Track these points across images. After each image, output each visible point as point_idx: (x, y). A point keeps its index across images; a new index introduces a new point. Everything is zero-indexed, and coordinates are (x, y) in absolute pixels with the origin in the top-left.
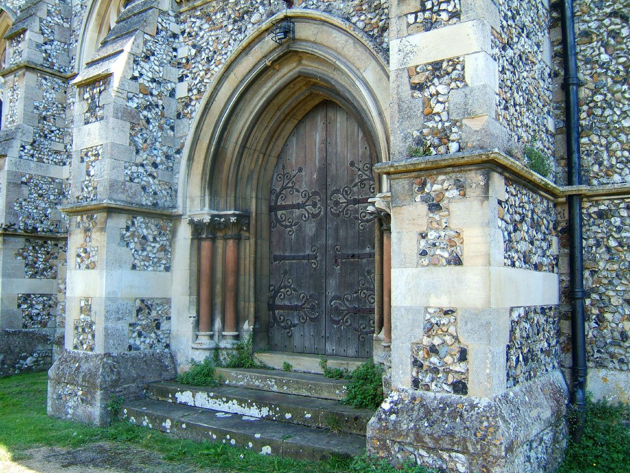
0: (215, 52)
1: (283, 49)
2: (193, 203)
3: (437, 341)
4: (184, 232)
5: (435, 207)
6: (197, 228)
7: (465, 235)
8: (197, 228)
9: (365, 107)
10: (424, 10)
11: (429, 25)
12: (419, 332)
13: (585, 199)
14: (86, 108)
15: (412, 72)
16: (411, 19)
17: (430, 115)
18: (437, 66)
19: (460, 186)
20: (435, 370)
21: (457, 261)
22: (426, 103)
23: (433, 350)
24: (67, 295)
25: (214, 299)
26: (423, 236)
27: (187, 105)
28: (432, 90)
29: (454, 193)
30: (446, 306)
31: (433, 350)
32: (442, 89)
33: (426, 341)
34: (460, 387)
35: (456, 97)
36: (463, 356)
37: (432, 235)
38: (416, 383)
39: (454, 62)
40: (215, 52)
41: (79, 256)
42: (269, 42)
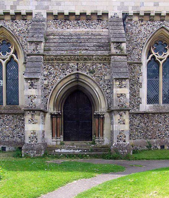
0: (56, 76)
1: (76, 79)
2: (51, 109)
3: (121, 135)
4: (48, 116)
5: (121, 116)
6: (52, 115)
7: (126, 120)
8: (52, 115)
9: (92, 93)
10: (120, 85)
11: (120, 87)
12: (118, 134)
13: (28, 117)
14: (29, 84)
15: (117, 94)
16: (118, 86)
17: (120, 102)
18: (122, 94)
19: (125, 113)
20: (121, 139)
21: (124, 124)
22: (120, 100)
23: (120, 136)
24: (26, 130)
25: (55, 132)
26: (119, 120)
27: (47, 86)
28: (121, 98)
29: (124, 114)
30: (122, 130)
31: (120, 136)
32: (122, 98)
33: (119, 135)
34: (124, 141)
35: (125, 100)
36: (125, 137)
37: (120, 120)
38: (118, 141)
39: (124, 94)
40: (56, 76)
41: (29, 121)
42: (73, 77)
